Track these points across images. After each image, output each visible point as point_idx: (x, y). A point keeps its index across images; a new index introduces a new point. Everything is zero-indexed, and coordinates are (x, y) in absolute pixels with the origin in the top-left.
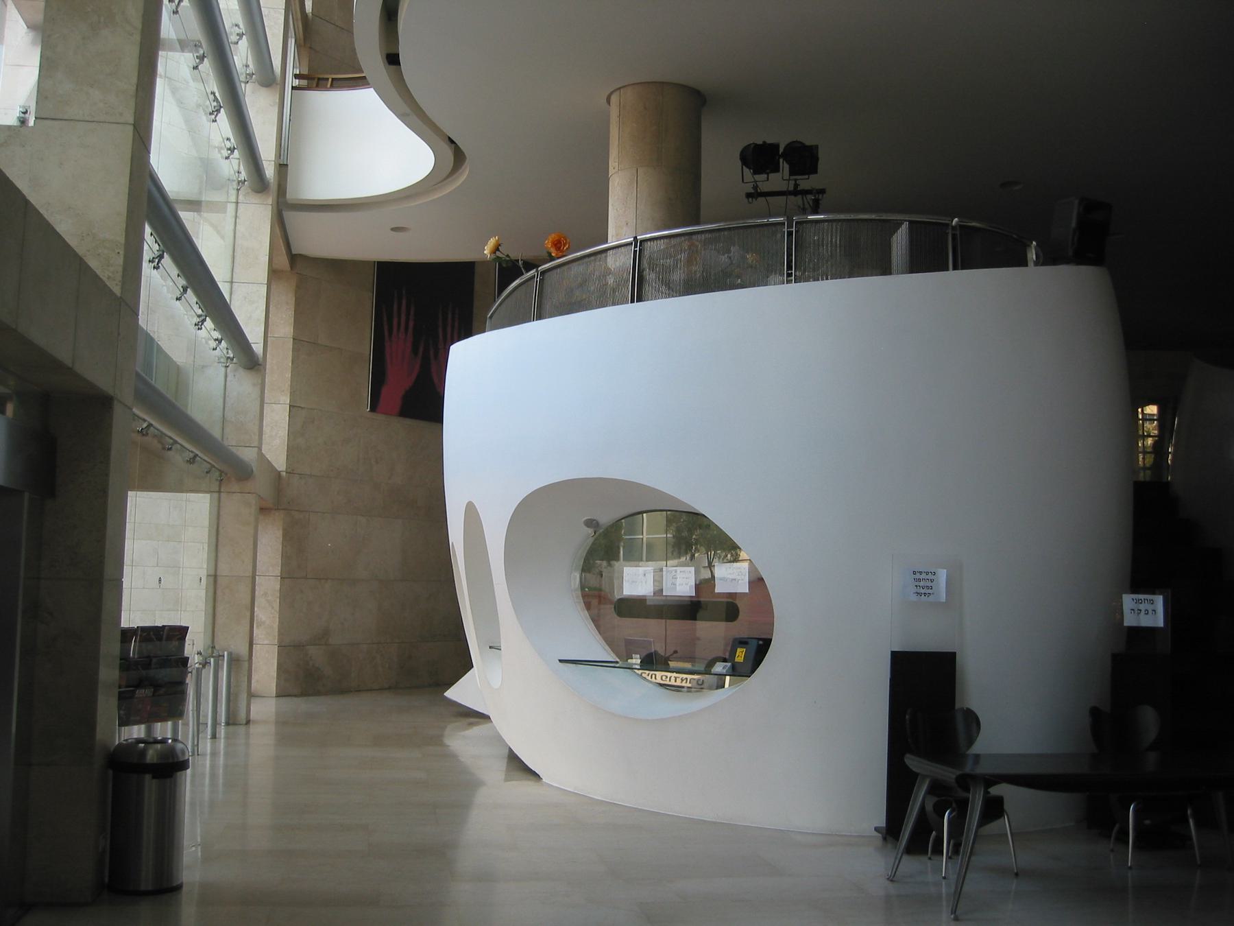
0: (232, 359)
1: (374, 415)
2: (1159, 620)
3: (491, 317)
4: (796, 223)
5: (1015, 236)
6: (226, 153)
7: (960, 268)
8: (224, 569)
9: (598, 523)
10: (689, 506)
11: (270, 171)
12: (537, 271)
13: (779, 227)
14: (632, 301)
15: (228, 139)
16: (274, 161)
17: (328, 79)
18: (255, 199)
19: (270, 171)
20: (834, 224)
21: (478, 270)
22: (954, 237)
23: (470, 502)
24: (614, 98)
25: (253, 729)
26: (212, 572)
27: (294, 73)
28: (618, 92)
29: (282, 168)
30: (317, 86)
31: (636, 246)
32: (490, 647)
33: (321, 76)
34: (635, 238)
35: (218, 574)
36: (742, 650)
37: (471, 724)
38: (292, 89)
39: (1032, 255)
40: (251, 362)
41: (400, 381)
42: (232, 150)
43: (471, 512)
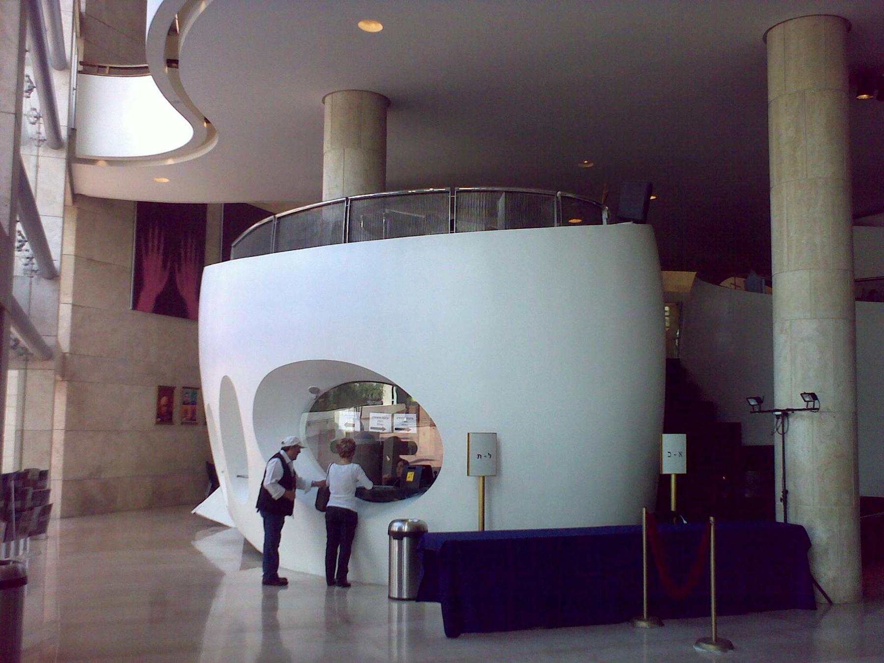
0: (36, 271)
1: (135, 312)
2: (408, 479)
3: (235, 246)
4: (457, 192)
5: (595, 203)
6: (33, 120)
7: (556, 223)
8: (29, 426)
9: (319, 390)
10: (387, 379)
11: (64, 133)
12: (275, 217)
13: (445, 194)
14: (345, 242)
15: (35, 109)
16: (67, 126)
17: (105, 67)
18: (53, 154)
19: (64, 133)
20: (482, 193)
21: (209, 209)
22: (558, 202)
23: (226, 376)
24: (328, 99)
25: (49, 541)
26: (19, 428)
27: (79, 60)
28: (330, 96)
29: (73, 132)
30: (98, 72)
31: (347, 204)
32: (238, 476)
33: (101, 65)
34: (347, 199)
35: (25, 428)
36: (411, 473)
37: (217, 531)
38: (77, 73)
39: (605, 216)
40: (53, 275)
41: (154, 286)
42: (38, 117)
43: (227, 385)
